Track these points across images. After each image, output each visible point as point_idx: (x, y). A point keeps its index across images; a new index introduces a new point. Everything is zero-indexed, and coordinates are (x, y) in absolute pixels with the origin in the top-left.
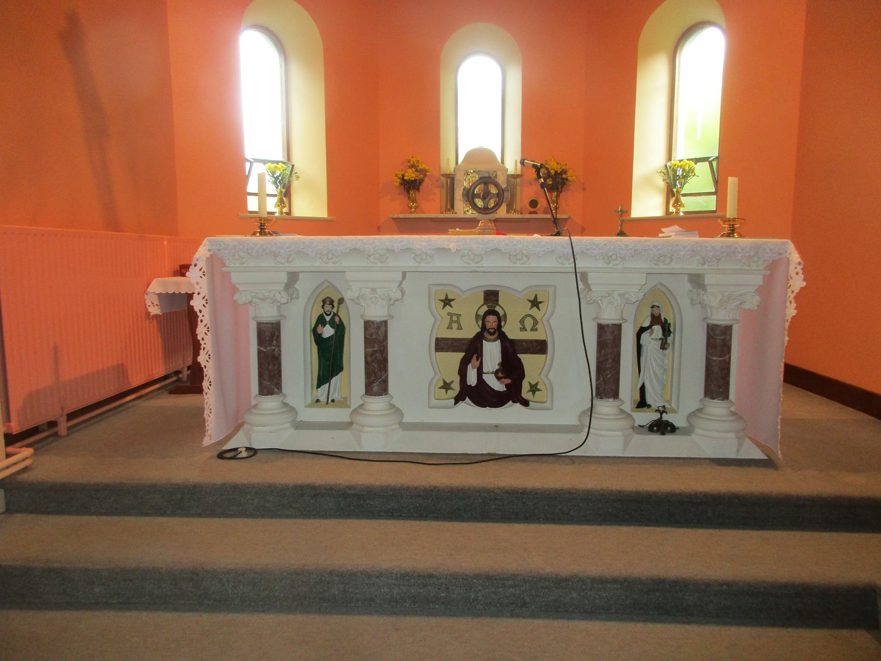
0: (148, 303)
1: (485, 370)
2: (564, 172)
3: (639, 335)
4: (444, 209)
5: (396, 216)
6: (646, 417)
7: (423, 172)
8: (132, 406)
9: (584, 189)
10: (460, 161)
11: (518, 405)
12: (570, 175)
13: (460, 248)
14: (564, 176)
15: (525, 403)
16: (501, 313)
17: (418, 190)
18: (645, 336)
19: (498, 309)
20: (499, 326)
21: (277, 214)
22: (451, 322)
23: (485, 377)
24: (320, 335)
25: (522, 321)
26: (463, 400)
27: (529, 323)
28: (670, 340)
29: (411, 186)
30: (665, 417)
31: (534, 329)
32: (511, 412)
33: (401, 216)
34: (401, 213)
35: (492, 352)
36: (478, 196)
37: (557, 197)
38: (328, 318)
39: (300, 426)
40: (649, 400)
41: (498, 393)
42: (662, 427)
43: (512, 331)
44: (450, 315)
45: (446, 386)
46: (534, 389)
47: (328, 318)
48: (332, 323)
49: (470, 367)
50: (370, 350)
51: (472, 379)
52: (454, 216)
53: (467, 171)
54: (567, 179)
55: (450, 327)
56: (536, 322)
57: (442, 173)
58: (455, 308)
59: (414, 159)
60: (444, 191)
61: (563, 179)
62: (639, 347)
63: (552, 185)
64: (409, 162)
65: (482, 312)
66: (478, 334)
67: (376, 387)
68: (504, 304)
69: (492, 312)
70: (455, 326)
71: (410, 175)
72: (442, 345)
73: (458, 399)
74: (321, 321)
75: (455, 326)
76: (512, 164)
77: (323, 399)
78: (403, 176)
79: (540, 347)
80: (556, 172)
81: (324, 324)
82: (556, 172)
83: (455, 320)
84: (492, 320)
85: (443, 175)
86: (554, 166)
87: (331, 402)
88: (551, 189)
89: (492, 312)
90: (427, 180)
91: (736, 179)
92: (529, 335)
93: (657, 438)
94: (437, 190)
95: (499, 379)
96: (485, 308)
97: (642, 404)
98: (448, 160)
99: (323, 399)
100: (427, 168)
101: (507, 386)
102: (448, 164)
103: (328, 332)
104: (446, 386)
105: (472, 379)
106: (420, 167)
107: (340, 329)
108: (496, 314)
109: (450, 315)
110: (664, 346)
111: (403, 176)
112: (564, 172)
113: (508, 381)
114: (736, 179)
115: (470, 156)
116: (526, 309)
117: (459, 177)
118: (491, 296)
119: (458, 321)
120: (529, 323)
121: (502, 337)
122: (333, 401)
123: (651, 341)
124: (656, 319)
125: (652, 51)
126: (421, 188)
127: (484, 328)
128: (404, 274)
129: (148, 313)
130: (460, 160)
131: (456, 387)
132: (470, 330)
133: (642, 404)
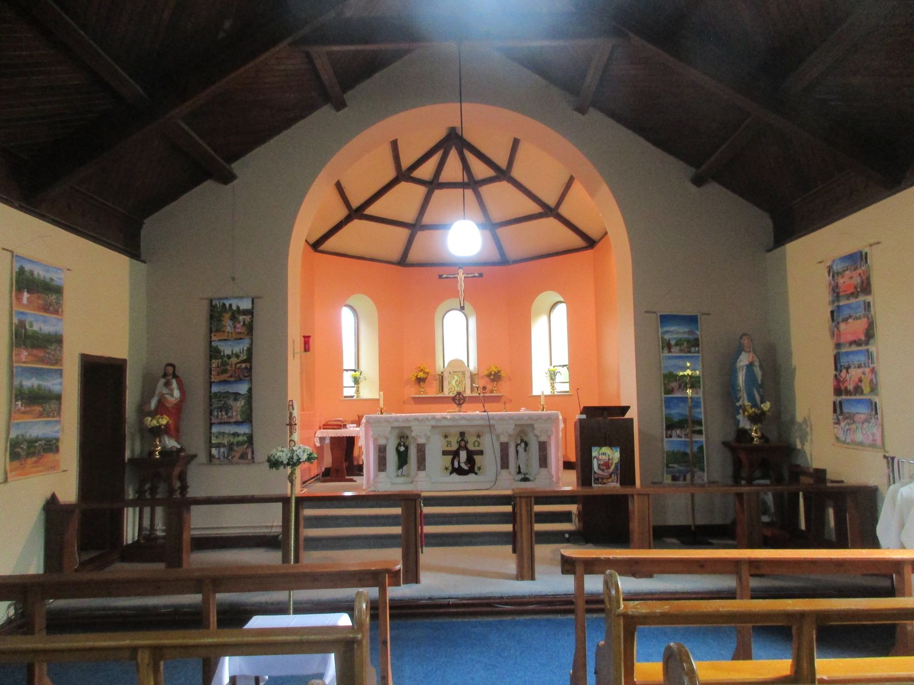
0: (315, 441)
1: (461, 462)
2: (499, 372)
3: (517, 447)
4: (438, 392)
5: (413, 396)
6: (521, 476)
7: (427, 373)
8: (310, 486)
9: (510, 380)
10: (446, 366)
11: (473, 474)
12: (503, 374)
13: (696, 478)
14: (499, 374)
15: (476, 474)
16: (466, 440)
17: (425, 382)
18: (519, 447)
19: (465, 439)
20: (466, 445)
21: (355, 398)
22: (448, 444)
23: (461, 464)
24: (399, 450)
25: (474, 443)
26: (453, 473)
27: (477, 444)
28: (528, 448)
29: (420, 381)
30: (527, 476)
31: (478, 446)
32: (471, 476)
33: (416, 396)
34: (415, 394)
35: (463, 455)
36: (459, 396)
37: (497, 384)
38: (402, 444)
39: (393, 484)
40: (522, 471)
41: (465, 470)
42: (525, 479)
43: (471, 447)
44: (447, 441)
45: (446, 469)
46: (479, 468)
47: (402, 444)
48: (404, 445)
49: (455, 461)
50: (419, 454)
51: (456, 465)
52: (443, 396)
53: (450, 372)
54: (501, 375)
55: (447, 446)
56: (479, 443)
57: (437, 373)
58: (449, 439)
59: (422, 367)
60: (438, 382)
61: (499, 375)
62: (517, 452)
63: (494, 378)
64: (420, 368)
65: (459, 440)
66: (458, 448)
67: (422, 468)
68: (467, 437)
69: (463, 440)
70: (449, 445)
71: (421, 375)
72: (445, 453)
73: (451, 473)
74: (399, 445)
75: (449, 445)
76: (473, 366)
77: (400, 474)
78: (417, 375)
79: (481, 453)
80: (495, 372)
81: (401, 446)
82: (495, 372)
83: (449, 444)
84: (463, 444)
85: (438, 375)
86: (494, 369)
87: (402, 475)
88: (493, 380)
89: (463, 440)
90: (429, 377)
91: (536, 392)
92: (477, 448)
93: (522, 483)
94: (434, 382)
95: (466, 465)
96: (460, 439)
97: (519, 472)
98: (440, 367)
99: (400, 474)
100: (429, 371)
101: (469, 467)
102: (439, 367)
103: (402, 449)
104: (446, 469)
105: (456, 465)
106: (426, 371)
107: (407, 448)
108: (464, 440)
109: (447, 441)
110: (525, 450)
111: (417, 375)
112: (499, 372)
113: (469, 465)
114: (536, 392)
115: (451, 363)
116: (475, 438)
117: (446, 375)
118: (462, 434)
119: (450, 444)
120: (477, 444)
121: (467, 449)
122: (404, 475)
123: (521, 449)
124: (522, 441)
125: (539, 314)
126: (426, 381)
127: (460, 446)
128: (253, 462)
129: (315, 445)
130: (446, 365)
131: (450, 468)
132: (454, 447)
133: (519, 472)
